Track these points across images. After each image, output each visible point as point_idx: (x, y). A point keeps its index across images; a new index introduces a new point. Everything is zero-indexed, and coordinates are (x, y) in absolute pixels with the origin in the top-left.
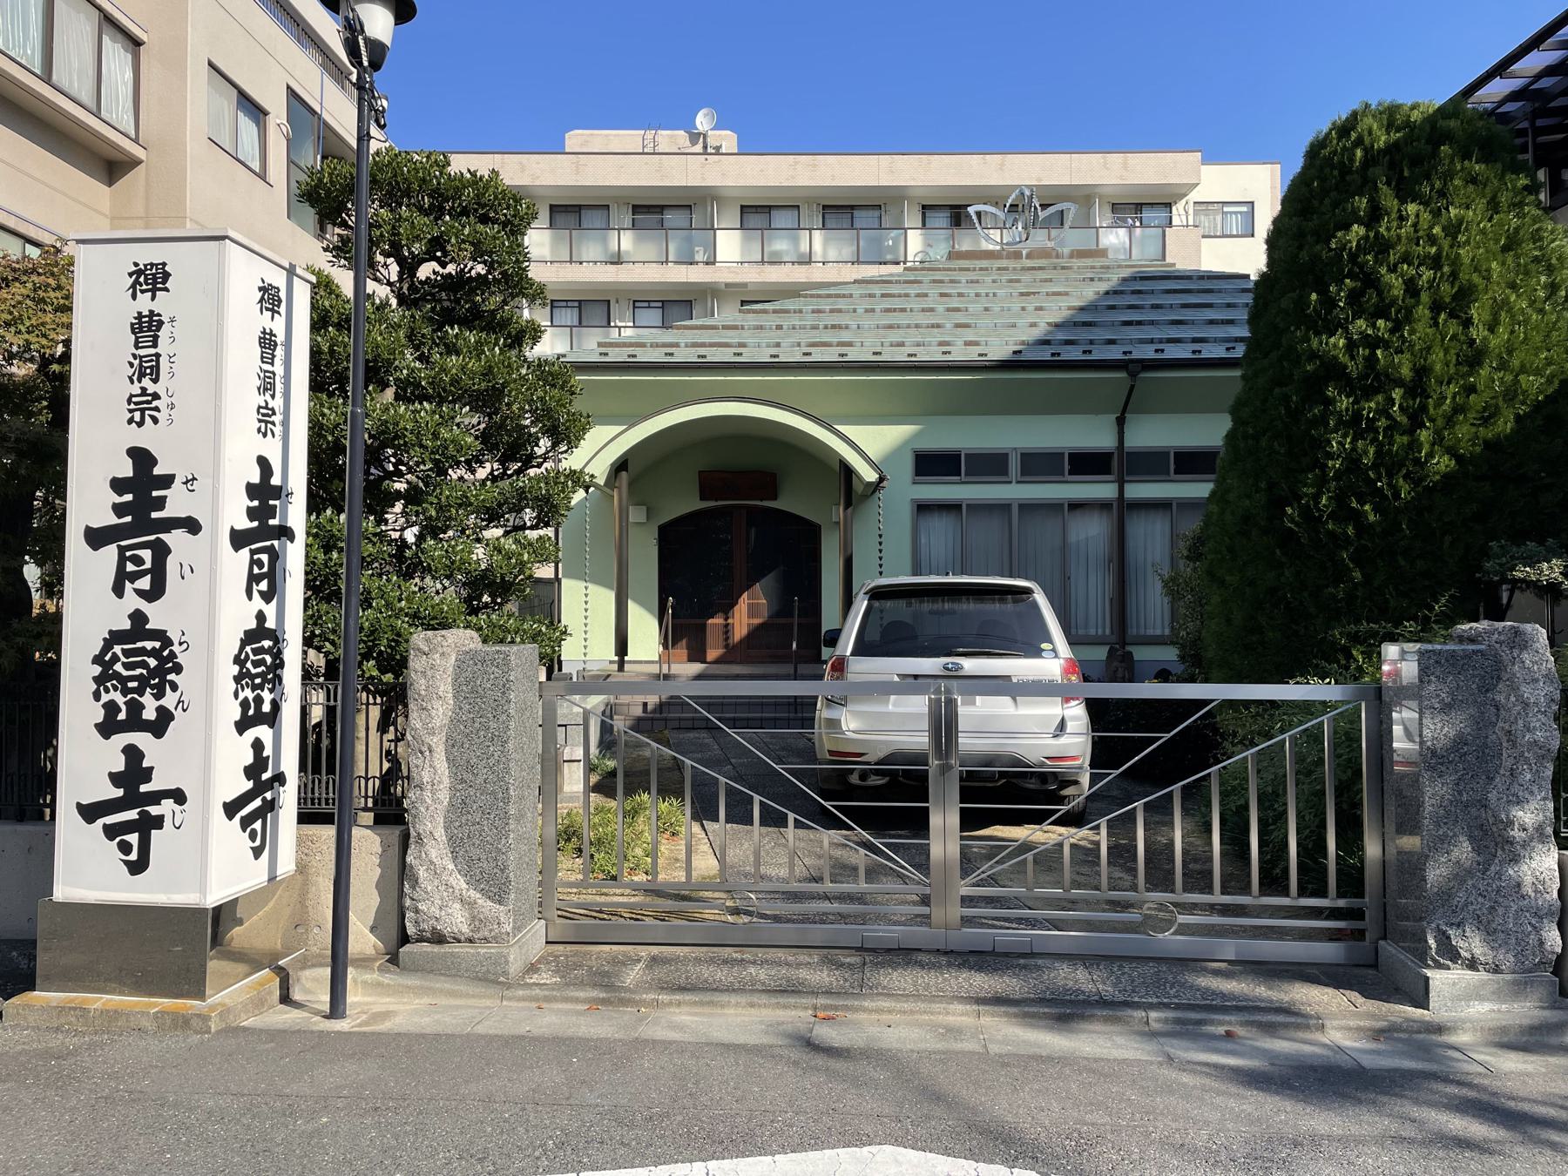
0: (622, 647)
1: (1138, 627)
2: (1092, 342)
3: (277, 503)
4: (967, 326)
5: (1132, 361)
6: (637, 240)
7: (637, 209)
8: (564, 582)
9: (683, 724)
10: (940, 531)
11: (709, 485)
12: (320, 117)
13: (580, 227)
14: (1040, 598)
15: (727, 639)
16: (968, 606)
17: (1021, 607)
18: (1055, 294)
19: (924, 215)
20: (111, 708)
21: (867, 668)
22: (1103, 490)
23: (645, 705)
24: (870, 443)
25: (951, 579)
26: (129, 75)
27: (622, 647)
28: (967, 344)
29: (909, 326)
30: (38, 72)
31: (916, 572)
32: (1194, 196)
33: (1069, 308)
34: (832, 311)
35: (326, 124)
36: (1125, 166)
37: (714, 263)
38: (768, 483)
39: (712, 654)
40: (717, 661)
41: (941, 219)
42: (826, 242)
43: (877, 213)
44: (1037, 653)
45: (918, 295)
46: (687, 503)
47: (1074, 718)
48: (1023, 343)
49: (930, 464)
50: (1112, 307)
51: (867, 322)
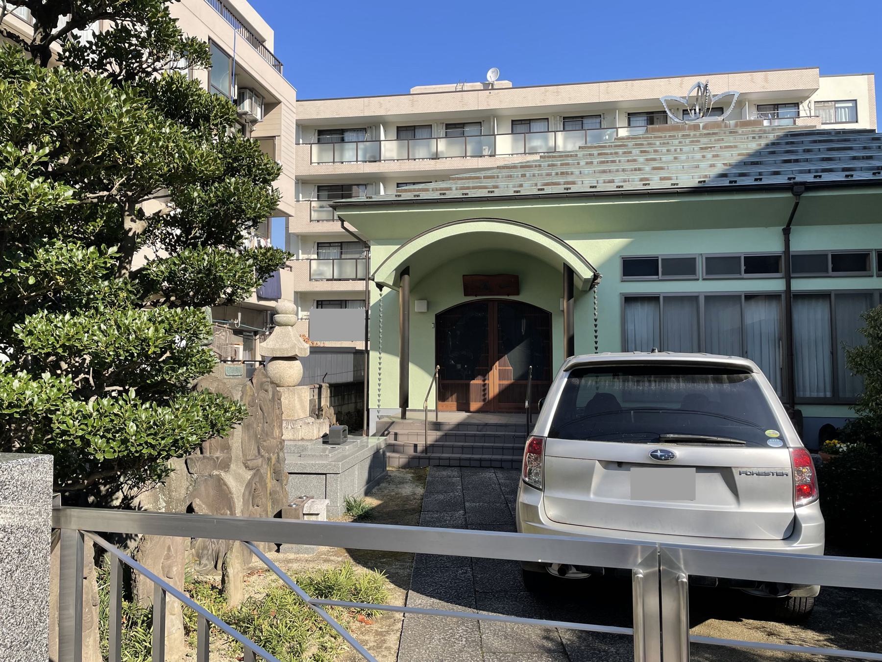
0: (404, 402)
1: (804, 391)
2: (760, 174)
4: (662, 168)
5: (796, 184)
6: (449, 145)
7: (448, 126)
8: (371, 353)
9: (442, 463)
10: (642, 315)
11: (470, 285)
12: (233, 59)
13: (414, 138)
14: (759, 377)
15: (484, 395)
16: (677, 386)
17: (737, 388)
18: (726, 147)
19: (629, 119)
21: (564, 452)
22: (773, 284)
23: (416, 446)
24: (592, 253)
25: (658, 356)
27: (404, 402)
28: (662, 179)
29: (617, 171)
30: (25, 18)
31: (625, 349)
32: (815, 97)
33: (739, 155)
34: (562, 165)
35: (237, 63)
36: (766, 80)
37: (494, 156)
38: (513, 283)
39: (475, 406)
40: (478, 411)
41: (641, 121)
42: (565, 139)
43: (598, 120)
44: (760, 441)
45: (624, 153)
46: (455, 298)
47: (809, 518)
48: (706, 176)
49: (633, 267)
50: (773, 153)
51: (586, 170)
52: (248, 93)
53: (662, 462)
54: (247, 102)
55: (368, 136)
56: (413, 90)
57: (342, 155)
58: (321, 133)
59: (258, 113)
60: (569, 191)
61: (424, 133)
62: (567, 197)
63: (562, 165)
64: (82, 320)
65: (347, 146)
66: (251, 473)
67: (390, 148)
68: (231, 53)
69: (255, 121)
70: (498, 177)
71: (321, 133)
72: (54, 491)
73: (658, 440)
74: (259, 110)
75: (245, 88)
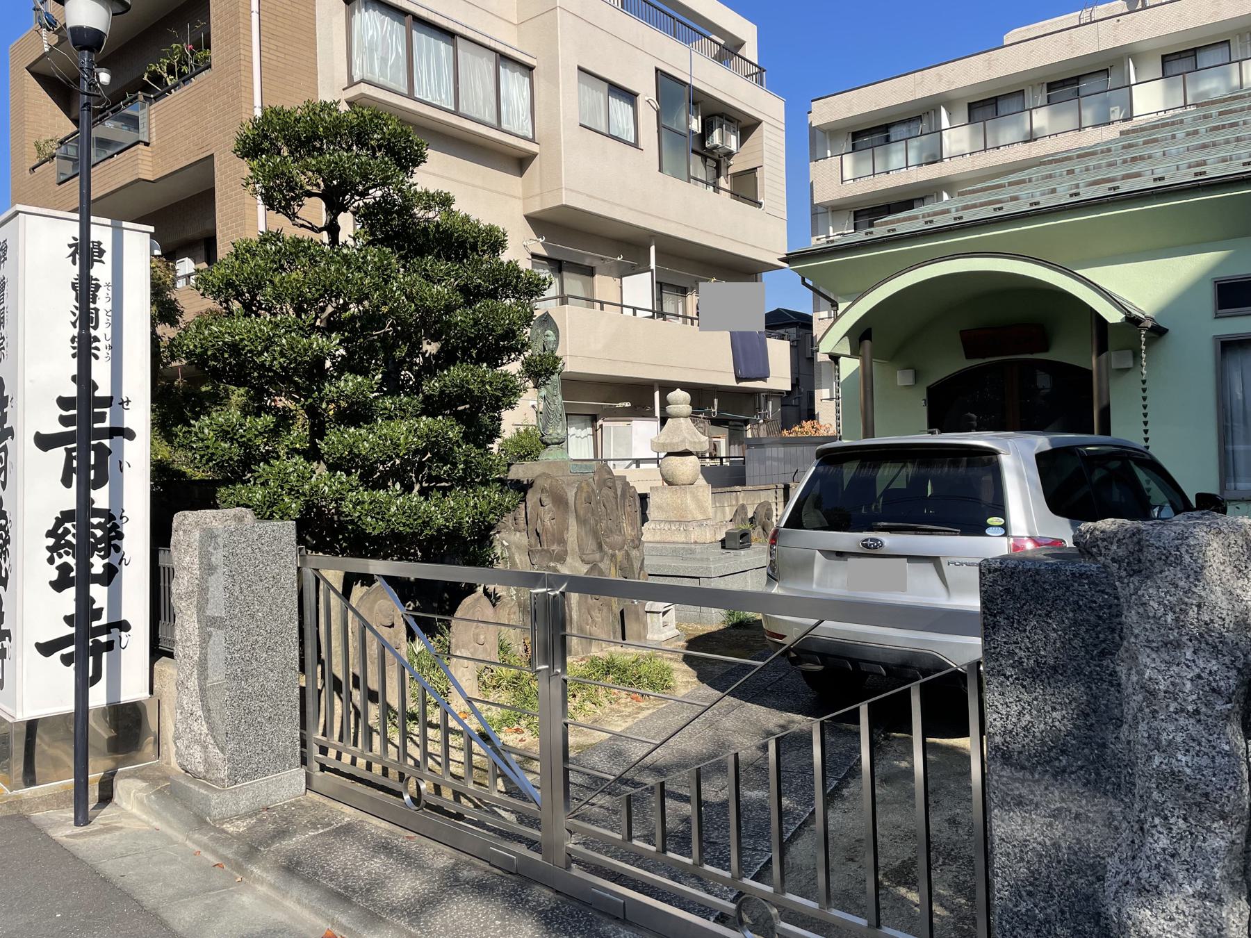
3: (107, 410)
6: (1053, 115)
11: (973, 343)
20: (64, 569)
26: (527, 93)
35: (694, 88)
38: (1039, 335)
52: (717, 120)
53: (871, 551)
54: (716, 133)
55: (924, 126)
56: (1009, 38)
57: (887, 162)
58: (856, 135)
59: (733, 142)
60: (1117, 192)
61: (1013, 104)
62: (1108, 202)
63: (1145, 143)
64: (363, 431)
65: (894, 147)
66: (588, 566)
67: (956, 137)
68: (687, 79)
69: (730, 154)
70: (1030, 180)
71: (856, 135)
72: (298, 543)
73: (871, 530)
74: (733, 138)
75: (714, 115)
